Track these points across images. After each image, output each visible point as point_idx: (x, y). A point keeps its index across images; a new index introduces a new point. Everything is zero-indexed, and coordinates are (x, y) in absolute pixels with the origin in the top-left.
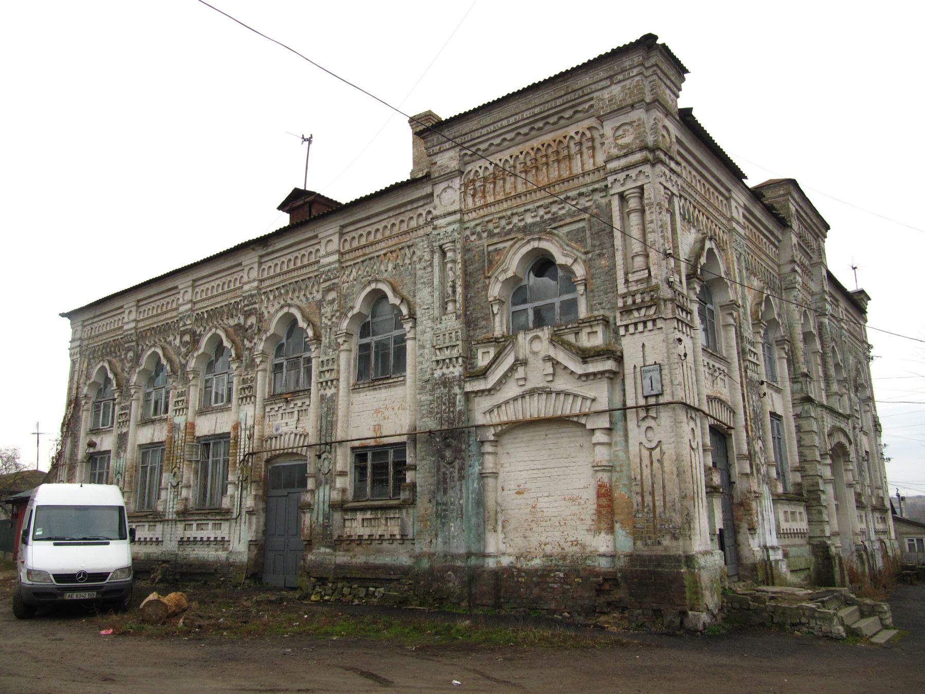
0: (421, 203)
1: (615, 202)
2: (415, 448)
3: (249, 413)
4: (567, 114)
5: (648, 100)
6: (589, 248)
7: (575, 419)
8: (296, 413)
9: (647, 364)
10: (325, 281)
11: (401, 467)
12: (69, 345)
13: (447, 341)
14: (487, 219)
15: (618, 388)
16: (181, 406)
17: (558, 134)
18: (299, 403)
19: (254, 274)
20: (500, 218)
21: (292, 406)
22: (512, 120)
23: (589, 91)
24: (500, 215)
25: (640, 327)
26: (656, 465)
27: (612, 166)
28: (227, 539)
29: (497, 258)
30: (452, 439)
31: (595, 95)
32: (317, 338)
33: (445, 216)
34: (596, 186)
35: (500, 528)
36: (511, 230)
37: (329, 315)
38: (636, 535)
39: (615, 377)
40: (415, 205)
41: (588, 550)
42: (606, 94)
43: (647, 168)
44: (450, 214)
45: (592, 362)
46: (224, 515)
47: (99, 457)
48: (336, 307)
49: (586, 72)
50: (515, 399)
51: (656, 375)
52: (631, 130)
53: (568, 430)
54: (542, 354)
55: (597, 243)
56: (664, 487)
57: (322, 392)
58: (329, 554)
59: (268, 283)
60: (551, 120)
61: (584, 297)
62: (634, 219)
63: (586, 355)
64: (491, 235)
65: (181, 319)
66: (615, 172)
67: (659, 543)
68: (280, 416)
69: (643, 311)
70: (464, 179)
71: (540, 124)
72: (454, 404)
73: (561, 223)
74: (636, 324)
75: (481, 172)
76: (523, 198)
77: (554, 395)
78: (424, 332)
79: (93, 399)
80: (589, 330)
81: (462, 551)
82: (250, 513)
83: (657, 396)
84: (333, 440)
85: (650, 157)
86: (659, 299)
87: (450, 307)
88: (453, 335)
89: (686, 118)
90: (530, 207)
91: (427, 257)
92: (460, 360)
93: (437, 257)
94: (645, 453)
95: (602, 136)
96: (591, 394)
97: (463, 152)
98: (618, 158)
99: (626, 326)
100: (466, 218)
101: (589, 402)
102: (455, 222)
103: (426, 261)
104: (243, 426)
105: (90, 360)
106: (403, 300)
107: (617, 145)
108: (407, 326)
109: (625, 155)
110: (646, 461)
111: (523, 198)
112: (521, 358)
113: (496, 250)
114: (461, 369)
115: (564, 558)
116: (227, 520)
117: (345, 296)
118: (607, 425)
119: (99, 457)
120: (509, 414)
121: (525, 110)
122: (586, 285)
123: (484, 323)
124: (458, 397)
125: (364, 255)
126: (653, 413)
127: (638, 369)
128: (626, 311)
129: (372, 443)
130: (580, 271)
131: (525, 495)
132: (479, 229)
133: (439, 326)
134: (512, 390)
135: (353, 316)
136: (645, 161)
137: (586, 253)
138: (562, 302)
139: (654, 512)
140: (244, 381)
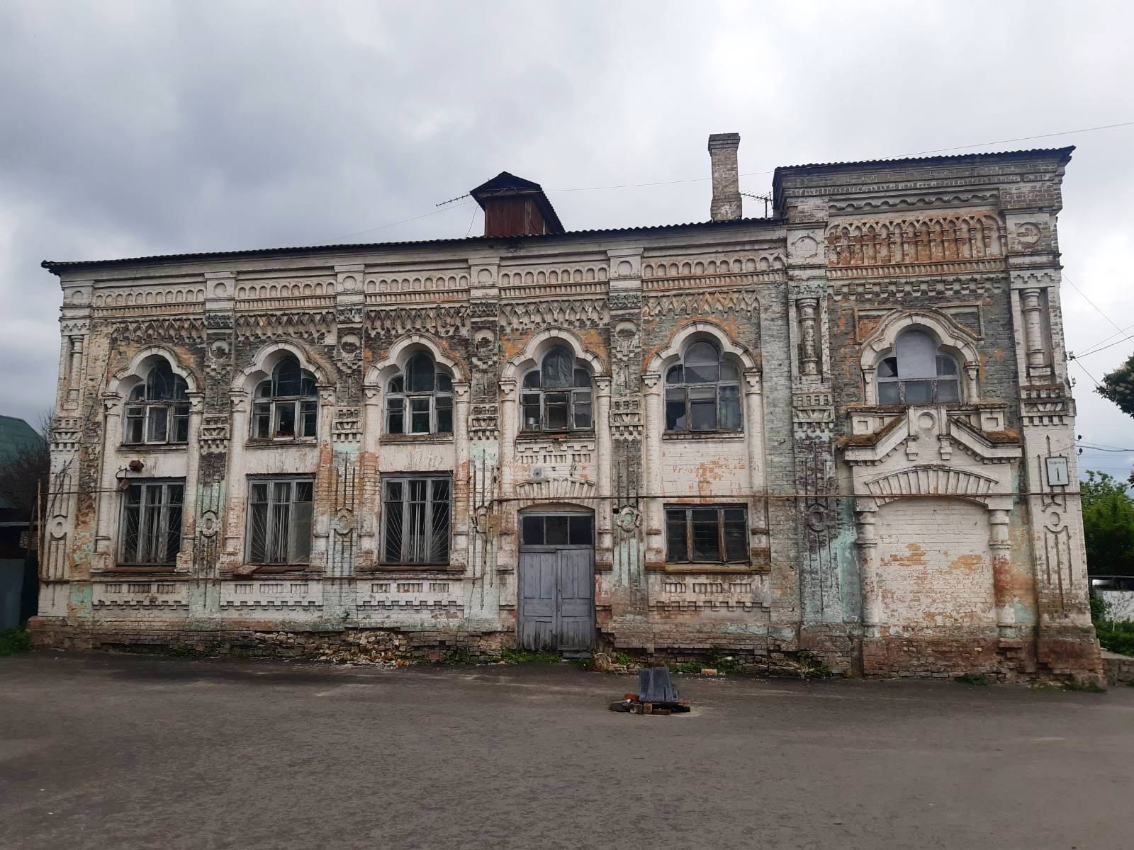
1: (1015, 297)
8: (570, 457)
9: (1052, 455)
13: (813, 402)
18: (577, 446)
21: (564, 447)
22: (901, 186)
23: (996, 181)
25: (1046, 421)
27: (1013, 261)
29: (871, 325)
30: (824, 509)
31: (1001, 187)
32: (608, 374)
33: (803, 267)
38: (1038, 609)
42: (1013, 189)
43: (1051, 272)
44: (812, 267)
45: (1001, 447)
49: (997, 162)
52: (1035, 231)
53: (961, 507)
54: (936, 432)
56: (1070, 566)
57: (617, 436)
62: (1035, 317)
63: (995, 441)
67: (1066, 616)
68: (541, 458)
69: (1049, 406)
72: (822, 471)
73: (949, 304)
78: (773, 389)
80: (989, 416)
83: (1063, 486)
84: (643, 492)
87: (811, 367)
88: (822, 398)
91: (777, 308)
92: (831, 426)
93: (793, 312)
94: (1051, 537)
97: (831, 204)
99: (1031, 418)
103: (774, 312)
104: (479, 465)
105: (114, 341)
109: (1032, 255)
110: (1051, 542)
111: (563, 288)
112: (912, 434)
115: (960, 628)
122: (977, 371)
124: (828, 463)
126: (1059, 500)
127: (1042, 460)
128: (1031, 403)
129: (697, 501)
132: (845, 290)
133: (799, 386)
139: (1061, 588)
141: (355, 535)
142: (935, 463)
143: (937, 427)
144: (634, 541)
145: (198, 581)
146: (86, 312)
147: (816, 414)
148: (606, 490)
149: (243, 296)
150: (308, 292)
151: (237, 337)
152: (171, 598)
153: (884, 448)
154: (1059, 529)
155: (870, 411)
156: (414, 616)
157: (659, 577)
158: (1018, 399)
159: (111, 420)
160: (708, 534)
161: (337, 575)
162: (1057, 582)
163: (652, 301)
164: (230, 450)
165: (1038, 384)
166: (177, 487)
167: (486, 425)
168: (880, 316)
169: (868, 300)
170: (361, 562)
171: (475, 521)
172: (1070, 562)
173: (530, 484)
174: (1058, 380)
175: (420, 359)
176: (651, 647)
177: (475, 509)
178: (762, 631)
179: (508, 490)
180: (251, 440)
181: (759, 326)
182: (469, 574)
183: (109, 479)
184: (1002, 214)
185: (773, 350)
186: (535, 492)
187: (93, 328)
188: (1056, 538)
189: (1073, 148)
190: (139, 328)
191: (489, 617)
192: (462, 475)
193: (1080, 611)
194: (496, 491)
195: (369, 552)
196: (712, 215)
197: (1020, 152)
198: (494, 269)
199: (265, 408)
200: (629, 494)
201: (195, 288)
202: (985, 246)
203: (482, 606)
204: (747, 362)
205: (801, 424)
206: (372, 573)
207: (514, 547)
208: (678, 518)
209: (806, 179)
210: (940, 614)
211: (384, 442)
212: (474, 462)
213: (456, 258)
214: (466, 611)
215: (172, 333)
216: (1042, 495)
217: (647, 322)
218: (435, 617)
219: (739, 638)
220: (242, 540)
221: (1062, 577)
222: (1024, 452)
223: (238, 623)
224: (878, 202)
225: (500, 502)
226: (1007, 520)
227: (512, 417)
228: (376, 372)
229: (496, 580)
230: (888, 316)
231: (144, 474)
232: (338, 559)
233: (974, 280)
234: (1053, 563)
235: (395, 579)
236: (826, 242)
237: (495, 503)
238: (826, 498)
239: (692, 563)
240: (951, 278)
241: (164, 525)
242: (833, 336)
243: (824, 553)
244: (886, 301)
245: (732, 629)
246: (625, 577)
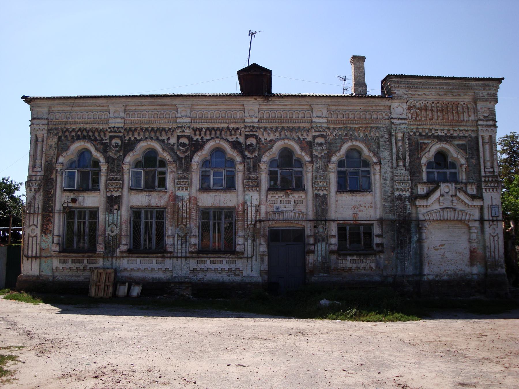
3: (254, 197)
10: (315, 131)
21: (290, 197)
26: (496, 242)
29: (425, 147)
36: (431, 135)
38: (486, 266)
41: (466, 272)
44: (401, 119)
46: (240, 255)
48: (324, 148)
52: (488, 111)
54: (450, 193)
56: (498, 250)
57: (316, 192)
58: (327, 276)
67: (497, 270)
78: (386, 173)
82: (262, 255)
83: (497, 217)
91: (386, 136)
94: (492, 238)
99: (486, 189)
102: (406, 124)
103: (385, 138)
104: (249, 204)
113: (424, 143)
114: (409, 194)
115: (457, 276)
116: (241, 258)
117: (330, 144)
123: (418, 174)
126: (495, 223)
127: (490, 206)
129: (352, 222)
131: (439, 251)
132: (414, 130)
138: (450, 173)
141: (188, 236)
143: (451, 191)
146: (46, 122)
148: (311, 216)
154: (495, 235)
156: (218, 275)
158: (481, 181)
160: (355, 237)
161: (179, 255)
164: (122, 193)
165: (488, 175)
166: (94, 213)
177: (247, 226)
181: (379, 144)
182: (245, 255)
189: (503, 79)
193: (502, 268)
194: (258, 216)
195: (195, 245)
200: (321, 217)
202: (469, 116)
203: (252, 271)
212: (246, 202)
216: (489, 220)
218: (229, 276)
222: (483, 203)
225: (260, 221)
226: (476, 231)
231: (77, 205)
232: (180, 247)
234: (492, 248)
235: (209, 258)
237: (258, 223)
242: (410, 151)
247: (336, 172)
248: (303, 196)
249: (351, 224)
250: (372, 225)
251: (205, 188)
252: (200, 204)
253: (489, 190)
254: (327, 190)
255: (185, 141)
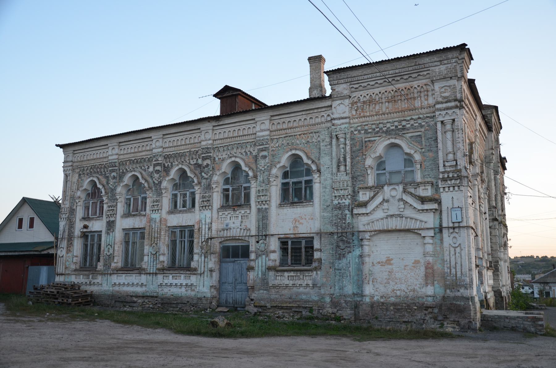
0: (323, 110)
1: (439, 125)
2: (321, 240)
4: (414, 76)
5: (459, 76)
6: (424, 146)
7: (416, 231)
8: (240, 217)
11: (310, 248)
12: (62, 165)
13: (341, 186)
14: (364, 124)
15: (437, 217)
16: (156, 208)
17: (407, 85)
18: (243, 212)
19: (209, 136)
20: (372, 124)
21: (237, 213)
24: (373, 123)
25: (451, 189)
27: (438, 106)
28: (195, 284)
29: (370, 145)
30: (346, 238)
31: (431, 68)
32: (255, 177)
33: (340, 119)
34: (428, 115)
35: (371, 282)
36: (379, 131)
37: (263, 165)
38: (446, 287)
39: (439, 211)
40: (319, 110)
42: (437, 69)
43: (457, 111)
47: (90, 235)
49: (427, 56)
50: (382, 219)
51: (459, 213)
52: (449, 90)
54: (398, 197)
55: (428, 144)
56: (461, 265)
57: (259, 207)
59: (218, 142)
60: (405, 77)
61: (419, 171)
62: (449, 135)
63: (423, 200)
64: (366, 132)
65: (154, 156)
66: (440, 110)
67: (458, 291)
69: (453, 181)
70: (351, 100)
71: (398, 78)
72: (345, 219)
73: (408, 132)
74: (449, 187)
75: (361, 98)
76: (392, 114)
77: (404, 218)
79: (84, 199)
80: (424, 188)
81: (350, 292)
83: (459, 222)
84: (267, 233)
85: (458, 104)
86: (461, 176)
87: (342, 168)
88: (345, 183)
89: (471, 83)
90: (391, 121)
91: (328, 140)
92: (349, 197)
93: (334, 141)
94: (452, 249)
95: (433, 90)
96: (424, 219)
97: (351, 86)
98: (442, 103)
100: (351, 121)
101: (423, 223)
102: (346, 123)
103: (326, 142)
104: (204, 222)
105: (80, 175)
106: (313, 162)
107: (441, 96)
108: (316, 176)
109: (446, 102)
110: (452, 252)
111: (386, 115)
115: (407, 297)
118: (433, 235)
119: (90, 235)
120: (378, 226)
121: (390, 71)
124: (348, 216)
125: (287, 134)
126: (457, 230)
127: (449, 209)
128: (444, 180)
129: (292, 236)
130: (417, 157)
132: (359, 128)
133: (336, 178)
134: (380, 214)
135: (280, 167)
136: (456, 107)
137: (422, 149)
139: (456, 276)
140: (203, 197)
142: (396, 213)
144: (264, 257)
145: (105, 274)
147: (343, 191)
148: (254, 232)
149: (122, 152)
150: (144, 149)
151: (119, 170)
152: (96, 281)
153: (371, 207)
154: (456, 245)
155: (370, 188)
157: (273, 273)
159: (78, 208)
160: (298, 252)
161: (151, 272)
162: (455, 273)
163: (275, 140)
167: (207, 204)
168: (375, 140)
169: (370, 132)
170: (159, 266)
171: (202, 248)
172: (461, 262)
173: (224, 230)
174: (459, 167)
175: (183, 174)
176: (269, 305)
177: (202, 243)
178: (316, 299)
179: (214, 234)
180: (124, 214)
181: (320, 149)
182: (199, 272)
183: (77, 232)
184: (433, 82)
185: (325, 161)
186: (225, 234)
187: (73, 170)
188: (455, 250)
190: (87, 169)
191: (206, 291)
192: (196, 227)
196: (310, 95)
197: (437, 50)
198: (210, 131)
199: (175, 196)
200: (263, 235)
201: (105, 151)
204: (314, 167)
205: (335, 196)
206: (162, 270)
207: (217, 260)
208: (286, 245)
209: (338, 75)
210: (399, 290)
211: (170, 212)
213: (196, 128)
214: (198, 288)
215: (98, 170)
217: (273, 150)
219: (307, 301)
220: (120, 257)
221: (457, 270)
223: (118, 292)
224: (365, 84)
225: (211, 239)
227: (217, 199)
228: (166, 182)
229: (209, 273)
230: (379, 140)
233: (419, 118)
234: (453, 263)
236: (350, 105)
238: (346, 233)
239: (303, 266)
240: (386, 121)
241: (95, 250)
242: (352, 151)
243: (344, 260)
244: (378, 132)
245: (304, 297)
246: (260, 273)
247: (280, 186)
248: (248, 212)
249: (292, 238)
250: (313, 238)
251: (174, 209)
252: (169, 225)
253: (449, 190)
254: (268, 204)
255: (158, 168)
